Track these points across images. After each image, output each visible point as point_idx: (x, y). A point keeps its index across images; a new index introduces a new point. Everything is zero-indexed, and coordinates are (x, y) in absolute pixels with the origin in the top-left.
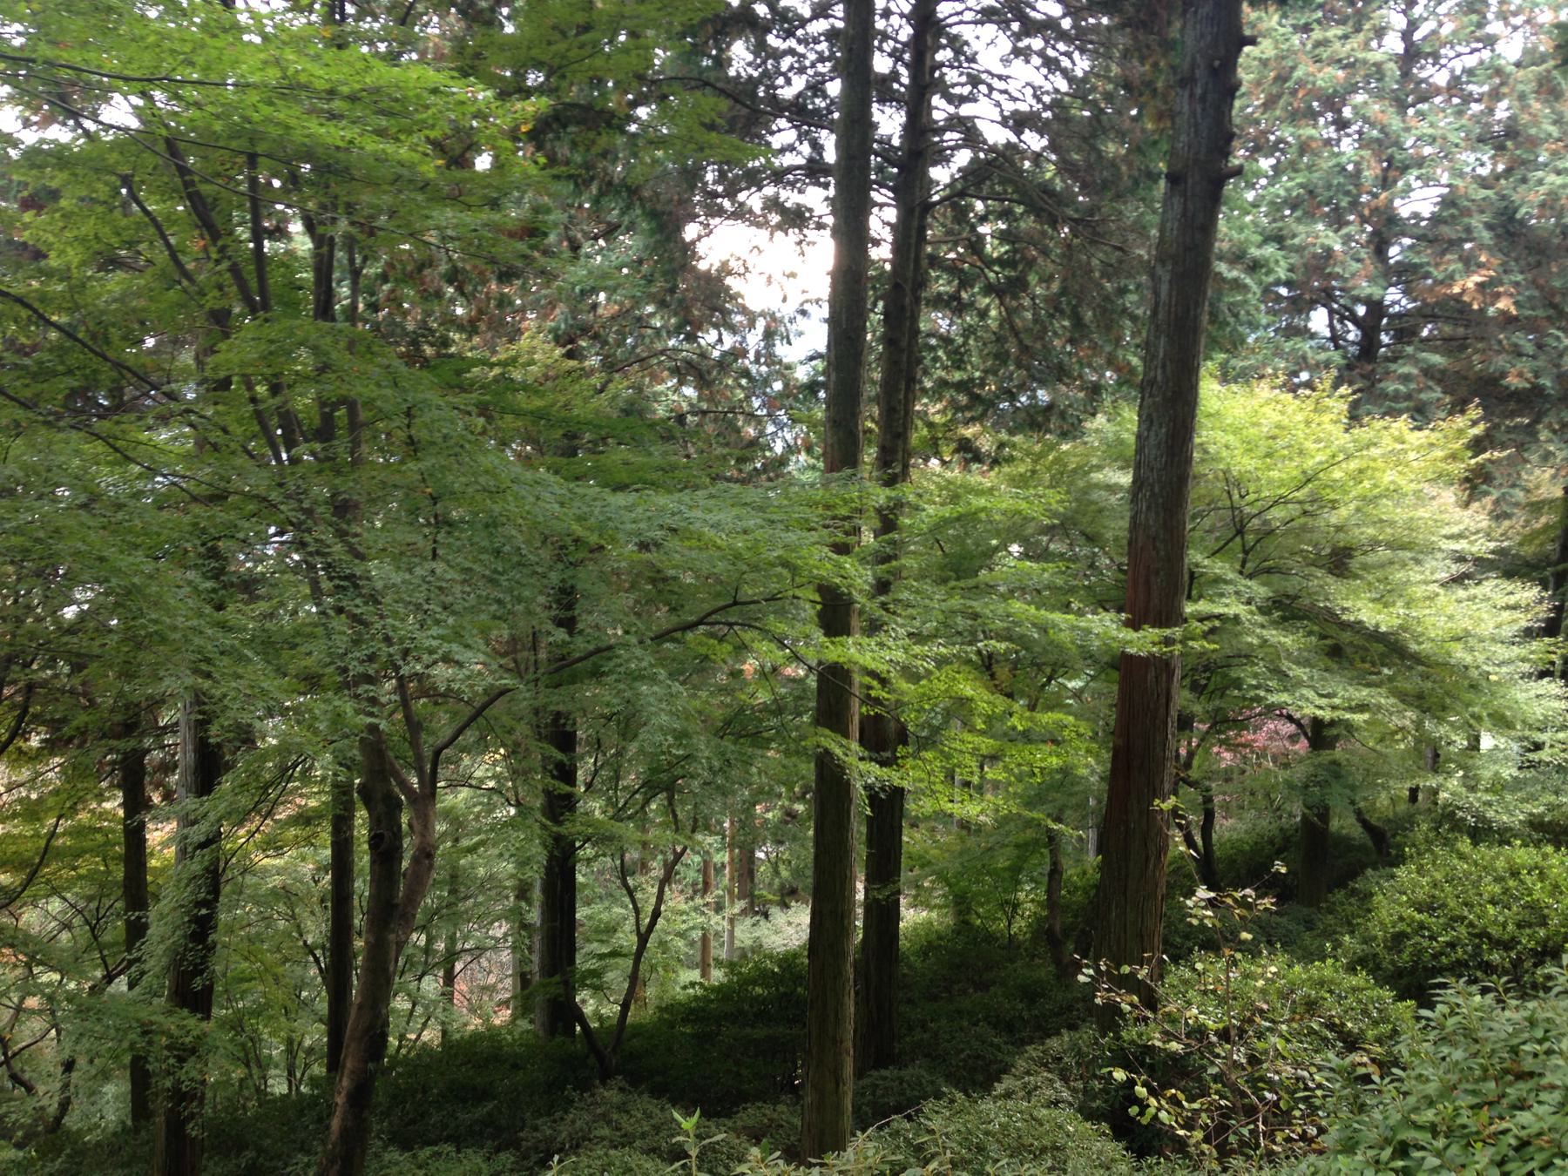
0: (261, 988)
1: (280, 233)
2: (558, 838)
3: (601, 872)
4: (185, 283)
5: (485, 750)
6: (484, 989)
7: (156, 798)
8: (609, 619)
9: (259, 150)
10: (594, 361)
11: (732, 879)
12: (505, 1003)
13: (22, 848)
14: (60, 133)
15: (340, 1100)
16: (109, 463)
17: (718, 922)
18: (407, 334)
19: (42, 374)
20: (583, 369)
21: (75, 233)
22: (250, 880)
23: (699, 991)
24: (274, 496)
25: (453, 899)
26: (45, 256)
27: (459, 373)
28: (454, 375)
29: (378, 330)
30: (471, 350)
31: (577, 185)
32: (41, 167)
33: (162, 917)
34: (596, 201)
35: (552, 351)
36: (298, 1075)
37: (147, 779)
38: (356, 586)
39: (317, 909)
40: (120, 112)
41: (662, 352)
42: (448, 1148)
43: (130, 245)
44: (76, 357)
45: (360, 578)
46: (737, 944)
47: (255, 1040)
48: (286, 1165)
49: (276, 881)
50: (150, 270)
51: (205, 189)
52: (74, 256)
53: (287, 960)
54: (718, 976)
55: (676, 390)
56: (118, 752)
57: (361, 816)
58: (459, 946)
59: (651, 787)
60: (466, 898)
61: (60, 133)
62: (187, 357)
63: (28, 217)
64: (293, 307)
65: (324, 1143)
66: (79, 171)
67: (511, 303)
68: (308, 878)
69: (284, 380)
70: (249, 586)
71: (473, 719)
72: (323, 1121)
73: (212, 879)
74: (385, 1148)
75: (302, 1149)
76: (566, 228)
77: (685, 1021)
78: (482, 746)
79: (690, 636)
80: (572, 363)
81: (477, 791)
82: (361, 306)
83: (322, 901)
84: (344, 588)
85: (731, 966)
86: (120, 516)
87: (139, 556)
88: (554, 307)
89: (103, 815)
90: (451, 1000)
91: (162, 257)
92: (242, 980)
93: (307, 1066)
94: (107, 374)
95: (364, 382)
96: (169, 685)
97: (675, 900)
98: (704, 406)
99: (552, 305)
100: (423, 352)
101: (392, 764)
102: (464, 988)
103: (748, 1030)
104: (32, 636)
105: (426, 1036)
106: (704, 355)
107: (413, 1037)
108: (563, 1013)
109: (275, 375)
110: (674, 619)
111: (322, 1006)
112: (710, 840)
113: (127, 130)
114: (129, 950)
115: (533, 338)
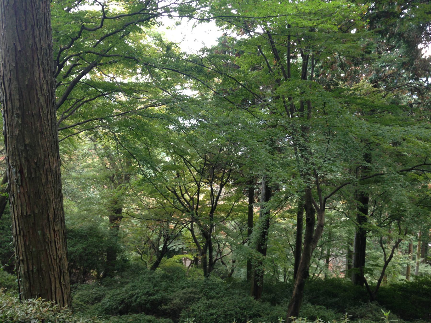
0: (278, 253)
1: (295, 57)
2: (361, 229)
3: (375, 241)
4: (270, 72)
5: (341, 200)
6: (338, 267)
7: (256, 201)
8: (383, 167)
9: (291, 34)
10: (382, 88)
11: (419, 251)
12: (342, 272)
13: (227, 208)
14: (246, 37)
15: (296, 286)
16: (250, 118)
17: (412, 263)
18: (326, 83)
19: (236, 96)
20: (379, 90)
21: (247, 61)
22: (276, 224)
23: (405, 283)
24: (287, 126)
25: (329, 240)
26: (240, 68)
27: (340, 93)
28: (339, 93)
29: (318, 82)
30: (344, 86)
31: (382, 35)
32: (240, 45)
33: (255, 230)
34: (388, 40)
35: (369, 85)
36: (287, 278)
37: (254, 195)
38: (306, 149)
39: (293, 236)
40: (259, 29)
41: (406, 85)
42: (324, 307)
43: (258, 63)
44: (245, 92)
45: (307, 147)
46: (419, 271)
47: (276, 266)
48: (282, 300)
49: (283, 226)
50: (262, 70)
51: (278, 48)
52: (246, 67)
53: (285, 247)
54: (412, 279)
55: (410, 96)
56: (248, 188)
57: (305, 213)
58: (331, 253)
59: (392, 218)
60: (333, 240)
61: (246, 37)
62: (269, 91)
63: (237, 58)
64: (296, 76)
65: (291, 296)
66: (249, 46)
67: (358, 72)
68: (291, 227)
69: (292, 97)
70: (280, 150)
71: (337, 190)
72: (291, 291)
73: (267, 223)
74: (307, 302)
75: (286, 297)
76: (377, 48)
77: (399, 290)
78: (339, 199)
79: (409, 173)
80: (376, 89)
81: (337, 212)
82: (314, 75)
83: (294, 233)
84: (303, 150)
85: (416, 277)
86: (251, 130)
87: (254, 141)
88: (371, 72)
89: (244, 203)
90: (328, 267)
91: (266, 66)
92: (274, 250)
93: (289, 276)
94: (251, 96)
95: (313, 96)
96: (260, 173)
97: (398, 253)
98: (420, 101)
99: (371, 72)
100: (331, 87)
101: (313, 200)
102: (332, 265)
103: (421, 298)
104: (231, 158)
105: (320, 276)
106: (421, 85)
107: (317, 275)
108: (360, 279)
109: (290, 95)
110: (404, 168)
111: (293, 261)
112: (412, 237)
113: (260, 33)
114: (248, 237)
115: (363, 82)
